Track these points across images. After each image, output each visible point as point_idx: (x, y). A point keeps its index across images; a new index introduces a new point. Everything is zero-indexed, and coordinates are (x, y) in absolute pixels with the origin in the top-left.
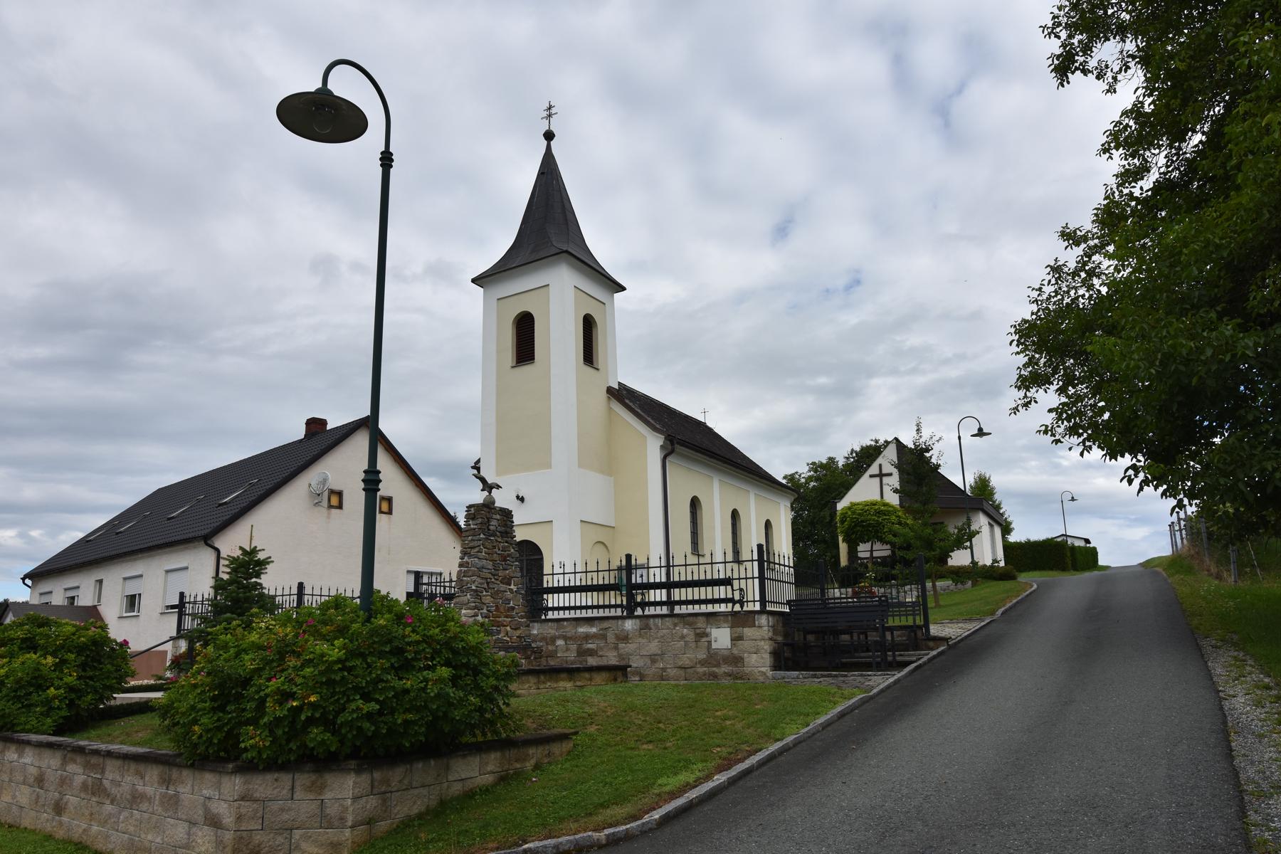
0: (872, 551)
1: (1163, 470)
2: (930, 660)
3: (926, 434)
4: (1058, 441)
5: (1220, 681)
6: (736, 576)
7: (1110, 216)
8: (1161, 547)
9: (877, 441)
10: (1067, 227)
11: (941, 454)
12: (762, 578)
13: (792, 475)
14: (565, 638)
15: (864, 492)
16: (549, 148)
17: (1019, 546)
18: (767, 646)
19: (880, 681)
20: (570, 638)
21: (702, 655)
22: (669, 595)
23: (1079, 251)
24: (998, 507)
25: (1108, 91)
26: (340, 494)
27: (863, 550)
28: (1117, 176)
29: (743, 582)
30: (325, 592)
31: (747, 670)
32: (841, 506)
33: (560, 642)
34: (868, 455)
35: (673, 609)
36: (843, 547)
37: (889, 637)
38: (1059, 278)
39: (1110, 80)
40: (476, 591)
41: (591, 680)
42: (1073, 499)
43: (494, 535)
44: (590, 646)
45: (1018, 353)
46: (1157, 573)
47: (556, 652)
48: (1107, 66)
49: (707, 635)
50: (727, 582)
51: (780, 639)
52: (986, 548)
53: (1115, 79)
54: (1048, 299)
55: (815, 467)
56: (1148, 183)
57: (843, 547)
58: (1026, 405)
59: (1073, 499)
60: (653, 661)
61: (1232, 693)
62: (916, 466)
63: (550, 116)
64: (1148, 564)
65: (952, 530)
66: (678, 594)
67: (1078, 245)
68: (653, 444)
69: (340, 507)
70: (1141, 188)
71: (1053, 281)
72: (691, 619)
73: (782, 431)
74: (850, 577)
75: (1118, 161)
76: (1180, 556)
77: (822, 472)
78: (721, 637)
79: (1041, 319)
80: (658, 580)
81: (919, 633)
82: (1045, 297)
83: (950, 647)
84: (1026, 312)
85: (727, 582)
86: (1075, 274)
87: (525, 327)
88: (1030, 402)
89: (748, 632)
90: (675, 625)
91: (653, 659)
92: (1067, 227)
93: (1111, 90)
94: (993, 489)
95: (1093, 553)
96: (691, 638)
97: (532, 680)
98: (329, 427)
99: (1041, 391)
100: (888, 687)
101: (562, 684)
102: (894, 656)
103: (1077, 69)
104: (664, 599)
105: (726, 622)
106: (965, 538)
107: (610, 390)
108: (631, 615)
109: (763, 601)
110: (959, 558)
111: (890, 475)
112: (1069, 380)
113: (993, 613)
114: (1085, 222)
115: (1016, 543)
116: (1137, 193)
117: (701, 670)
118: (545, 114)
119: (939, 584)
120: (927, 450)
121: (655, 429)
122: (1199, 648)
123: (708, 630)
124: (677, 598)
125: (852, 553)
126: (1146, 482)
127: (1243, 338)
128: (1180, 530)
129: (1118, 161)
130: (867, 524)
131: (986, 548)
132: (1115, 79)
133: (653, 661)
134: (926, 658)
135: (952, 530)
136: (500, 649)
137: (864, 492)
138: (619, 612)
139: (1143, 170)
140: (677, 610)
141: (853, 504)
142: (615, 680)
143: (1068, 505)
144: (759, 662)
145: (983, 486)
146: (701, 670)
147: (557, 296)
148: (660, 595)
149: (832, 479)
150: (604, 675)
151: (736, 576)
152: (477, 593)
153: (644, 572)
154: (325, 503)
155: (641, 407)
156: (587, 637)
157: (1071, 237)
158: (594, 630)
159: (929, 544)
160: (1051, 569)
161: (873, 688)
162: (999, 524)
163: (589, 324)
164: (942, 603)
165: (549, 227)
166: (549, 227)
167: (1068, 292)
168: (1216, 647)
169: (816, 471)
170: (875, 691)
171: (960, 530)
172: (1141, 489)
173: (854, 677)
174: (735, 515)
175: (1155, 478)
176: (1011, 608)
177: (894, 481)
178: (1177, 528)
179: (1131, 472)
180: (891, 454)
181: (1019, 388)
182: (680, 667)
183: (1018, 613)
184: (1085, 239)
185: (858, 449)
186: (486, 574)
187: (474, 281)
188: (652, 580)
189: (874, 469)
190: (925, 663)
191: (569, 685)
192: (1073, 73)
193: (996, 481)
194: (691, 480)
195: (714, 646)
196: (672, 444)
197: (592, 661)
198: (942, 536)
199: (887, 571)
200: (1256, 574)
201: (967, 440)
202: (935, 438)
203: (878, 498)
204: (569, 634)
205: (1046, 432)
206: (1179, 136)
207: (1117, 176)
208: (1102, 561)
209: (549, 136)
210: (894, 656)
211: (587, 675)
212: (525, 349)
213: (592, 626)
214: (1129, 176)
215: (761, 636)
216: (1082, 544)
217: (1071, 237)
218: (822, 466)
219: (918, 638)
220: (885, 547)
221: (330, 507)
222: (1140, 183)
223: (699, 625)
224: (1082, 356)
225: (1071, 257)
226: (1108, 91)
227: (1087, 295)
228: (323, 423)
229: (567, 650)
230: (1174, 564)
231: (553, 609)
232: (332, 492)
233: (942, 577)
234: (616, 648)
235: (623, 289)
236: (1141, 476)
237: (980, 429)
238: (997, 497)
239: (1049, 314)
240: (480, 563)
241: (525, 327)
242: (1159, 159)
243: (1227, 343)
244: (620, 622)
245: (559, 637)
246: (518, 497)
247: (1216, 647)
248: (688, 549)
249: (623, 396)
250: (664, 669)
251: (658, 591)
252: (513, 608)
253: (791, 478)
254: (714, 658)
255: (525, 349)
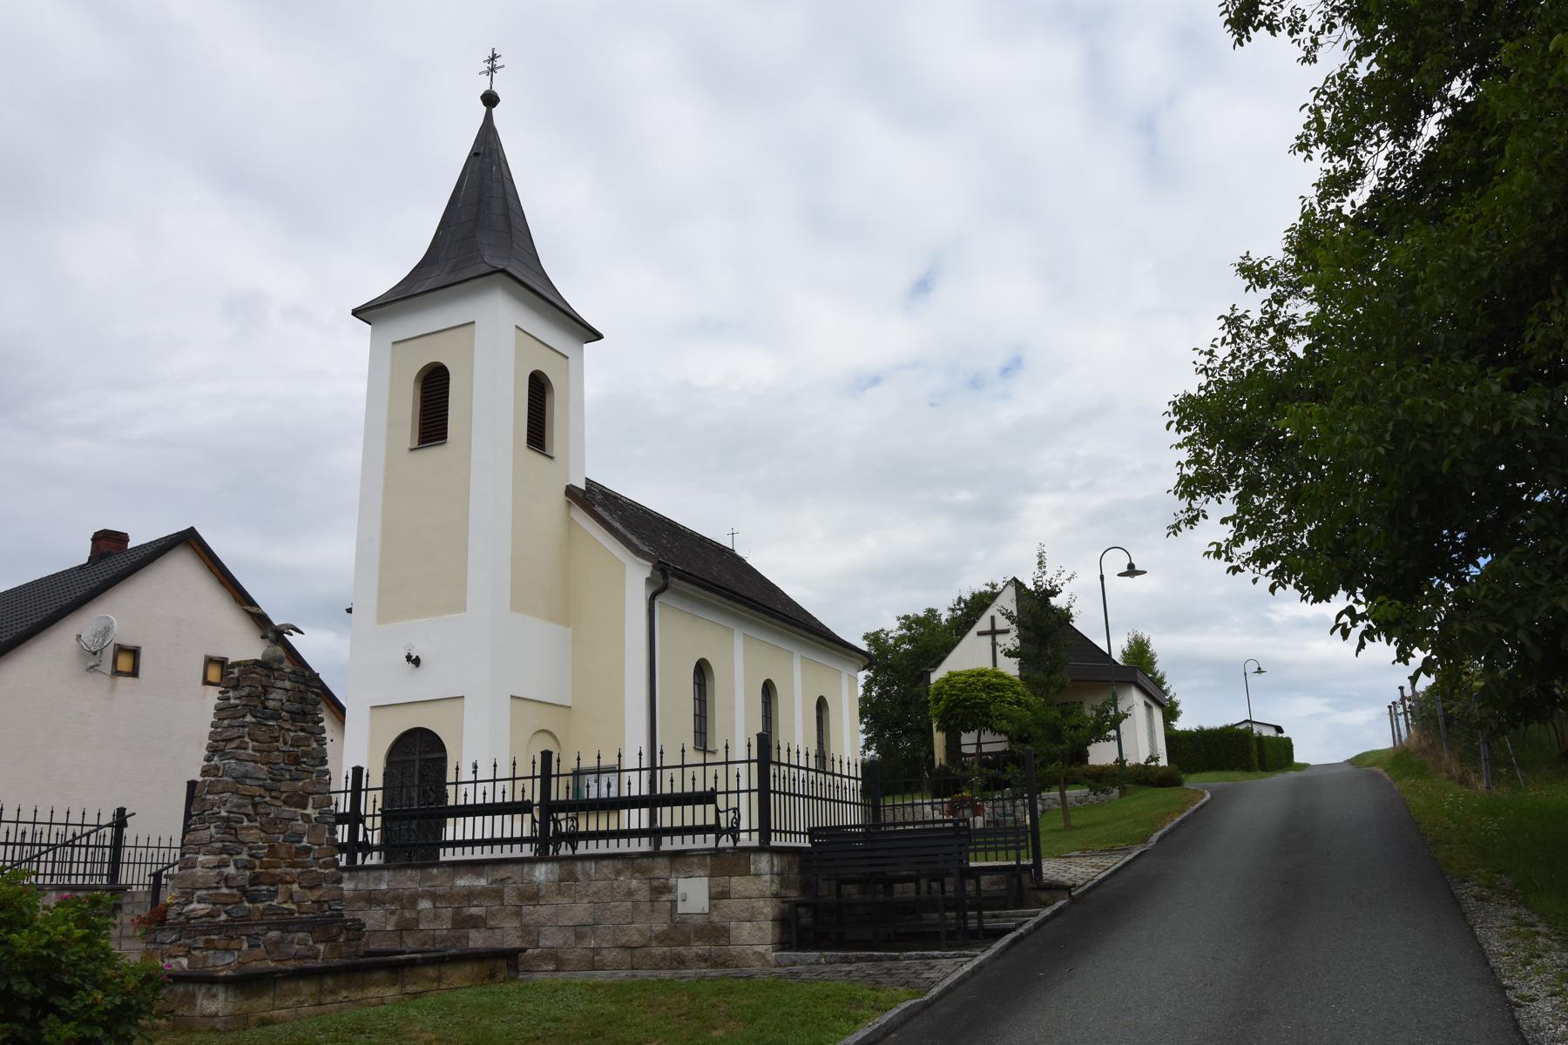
0: (979, 744)
1: (1394, 621)
2: (1038, 926)
3: (1051, 572)
4: (1235, 569)
5: (1501, 964)
6: (721, 787)
7: (1310, 240)
8: (1380, 738)
9: (993, 586)
10: (1247, 257)
11: (1073, 598)
12: (764, 791)
13: (876, 634)
14: (434, 897)
15: (970, 656)
16: (489, 118)
17: (1188, 736)
18: (768, 909)
19: (949, 969)
20: (443, 897)
21: (660, 925)
22: (652, 818)
23: (1267, 292)
24: (1159, 682)
25: (1305, 59)
26: (135, 653)
27: (968, 740)
28: (1318, 185)
29: (732, 797)
30: (76, 818)
31: (734, 950)
32: (936, 676)
33: (425, 904)
34: (979, 604)
35: (658, 843)
36: (939, 739)
37: (970, 886)
38: (1237, 335)
39: (1309, 44)
40: (227, 819)
41: (439, 979)
42: (1259, 671)
43: (275, 715)
44: (474, 910)
45: (1179, 446)
46: (1376, 775)
47: (417, 921)
48: (1304, 18)
49: (668, 889)
50: (708, 797)
51: (793, 894)
52: (1140, 739)
53: (1315, 41)
54: (1222, 367)
55: (908, 622)
56: (1360, 196)
57: (939, 739)
58: (1192, 521)
59: (1259, 671)
60: (580, 937)
61: (1525, 992)
62: (1040, 618)
63: (492, 70)
64: (1357, 761)
65: (1089, 713)
66: (669, 816)
67: (1263, 286)
68: (635, 575)
69: (134, 673)
70: (1353, 203)
71: (1229, 339)
72: (645, 862)
73: (854, 567)
74: (946, 785)
75: (1319, 164)
76: (1407, 750)
77: (918, 630)
78: (693, 893)
79: (1212, 396)
80: (635, 792)
81: (1026, 879)
82: (1217, 363)
83: (1074, 900)
84: (1192, 384)
85: (708, 797)
86: (1260, 329)
87: (434, 387)
88: (1196, 518)
89: (738, 883)
90: (618, 873)
91: (579, 932)
92: (1247, 257)
93: (1310, 58)
94: (1153, 655)
95: (1286, 746)
96: (643, 894)
97: (307, 988)
98: (130, 545)
99: (1213, 501)
100: (961, 981)
101: (373, 992)
102: (980, 917)
103: (1261, 24)
104: (645, 825)
105: (702, 866)
106: (1108, 724)
107: (571, 492)
108: (542, 857)
109: (765, 830)
110: (1101, 754)
111: (1006, 632)
112: (1253, 485)
113: (1145, 840)
114: (1272, 249)
115: (1184, 732)
116: (1347, 210)
117: (658, 950)
118: (486, 66)
119: (1073, 793)
120: (1054, 593)
121: (638, 552)
122: (1456, 901)
123: (672, 881)
124: (666, 824)
125: (953, 746)
126: (1368, 634)
127: (1518, 399)
128: (1405, 713)
129: (1319, 164)
130: (972, 703)
131: (1140, 739)
132: (1315, 41)
133: (580, 937)
134: (1033, 921)
135: (1089, 713)
136: (271, 926)
137: (970, 656)
138: (527, 851)
139: (1358, 173)
140: (667, 844)
141: (952, 675)
142: (492, 976)
143: (1254, 679)
144: (755, 936)
145: (1140, 653)
146: (658, 950)
147: (489, 340)
148: (637, 818)
149: (932, 636)
150: (469, 969)
151: (722, 788)
152: (228, 825)
153: (613, 778)
154: (107, 666)
155: (622, 520)
156: (470, 895)
157: (1253, 273)
158: (483, 882)
159: (1055, 734)
160: (1232, 769)
161: (934, 983)
162: (1161, 705)
163: (538, 387)
164: (1074, 822)
165: (482, 233)
166: (482, 233)
167: (1250, 356)
168: (1482, 899)
169: (909, 628)
170: (935, 991)
171: (1099, 712)
172: (1362, 645)
173: (909, 961)
174: (768, 689)
175: (1383, 627)
176: (1171, 830)
177: (1010, 641)
178: (1400, 710)
179: (1345, 619)
180: (1008, 601)
181: (1181, 497)
182: (625, 947)
183: (1184, 838)
184: (1273, 277)
185: (968, 597)
186: (252, 787)
187: (355, 313)
188: (625, 793)
189: (983, 624)
190: (1029, 932)
191: (390, 993)
192: (1256, 29)
193: (1154, 647)
194: (694, 633)
195: (681, 908)
196: (665, 576)
197: (477, 940)
198: (1074, 721)
199: (996, 774)
200: (1515, 777)
201: (1113, 581)
202: (1065, 576)
203: (990, 666)
204: (440, 891)
205: (1218, 554)
206: (1405, 130)
207: (1318, 185)
208: (1298, 758)
209: (490, 100)
210: (980, 917)
211: (431, 972)
212: (432, 422)
213: (479, 875)
214: (1336, 185)
215: (759, 887)
216: (1272, 733)
217: (1253, 273)
218: (918, 621)
219: (1024, 886)
220: (998, 738)
221: (116, 673)
222: (1352, 196)
223: (658, 873)
224: (1273, 448)
225: (1254, 304)
226: (1305, 59)
227: (1277, 360)
228: (122, 538)
229: (437, 917)
230: (1398, 760)
231: (455, 844)
232: (121, 649)
233: (1076, 782)
234: (518, 914)
235: (599, 336)
236: (1362, 625)
237: (1131, 566)
238: (1159, 667)
239: (1223, 389)
240: (238, 768)
241: (434, 387)
242: (1377, 159)
243: (1493, 407)
244: (526, 868)
245: (423, 896)
246: (409, 658)
247: (1482, 899)
248: (690, 743)
249: (594, 501)
250: (597, 951)
251: (634, 812)
252: (307, 850)
253: (874, 638)
254: (680, 930)
255: (432, 422)
